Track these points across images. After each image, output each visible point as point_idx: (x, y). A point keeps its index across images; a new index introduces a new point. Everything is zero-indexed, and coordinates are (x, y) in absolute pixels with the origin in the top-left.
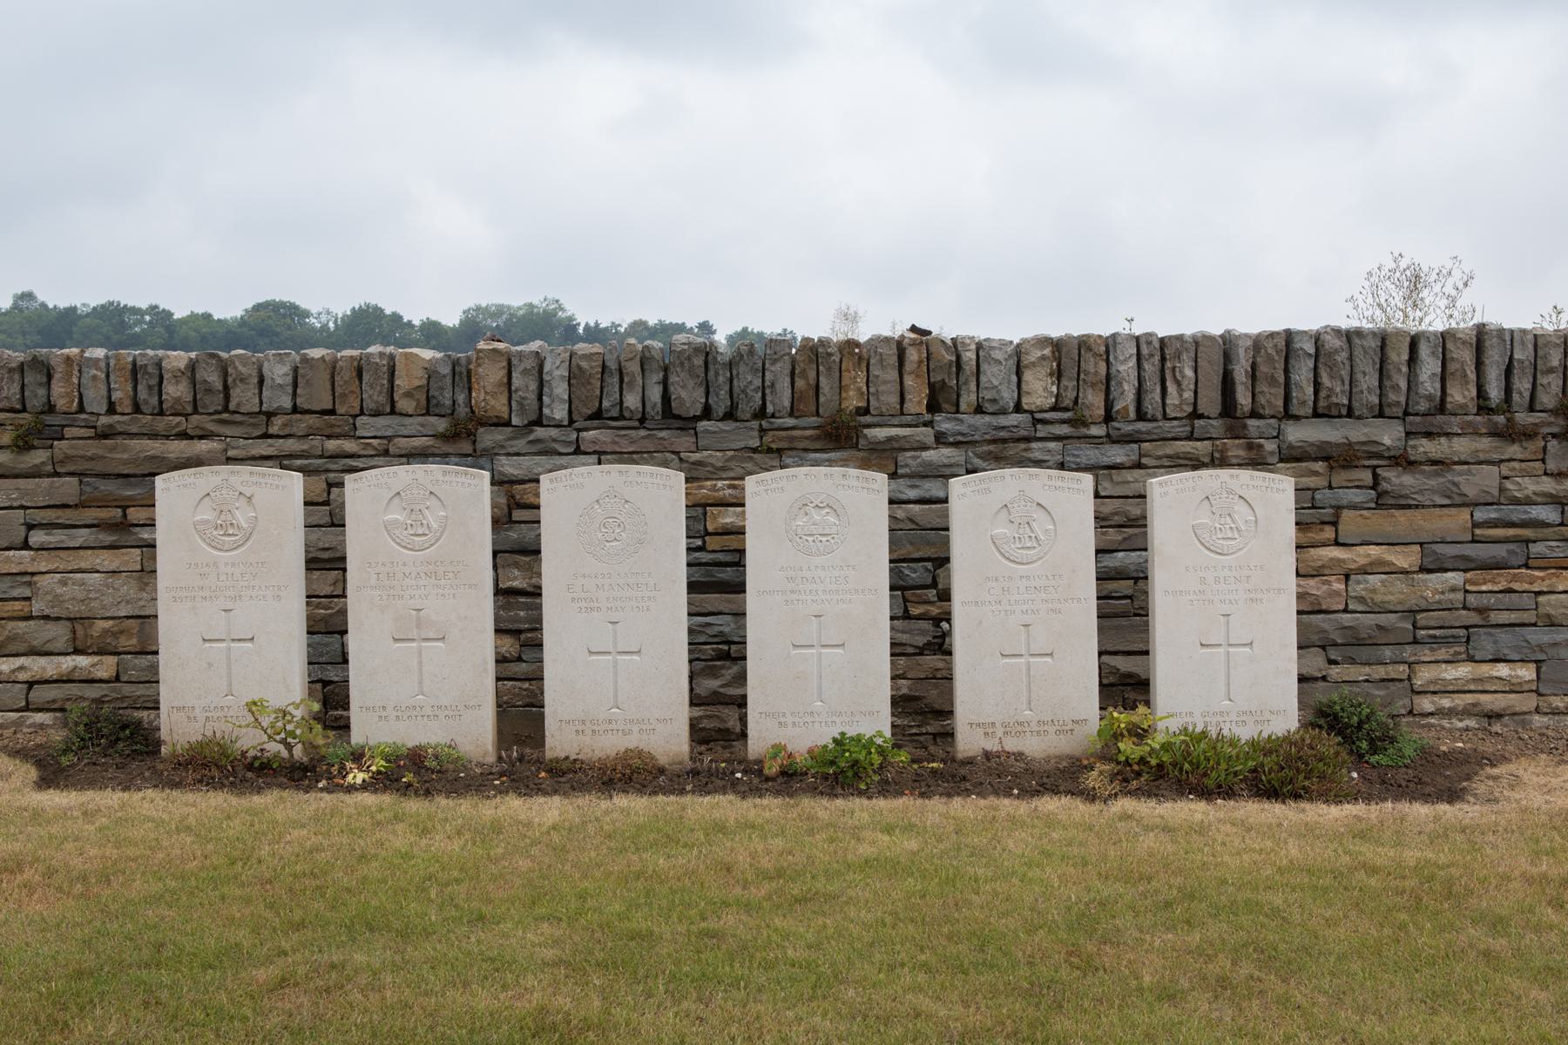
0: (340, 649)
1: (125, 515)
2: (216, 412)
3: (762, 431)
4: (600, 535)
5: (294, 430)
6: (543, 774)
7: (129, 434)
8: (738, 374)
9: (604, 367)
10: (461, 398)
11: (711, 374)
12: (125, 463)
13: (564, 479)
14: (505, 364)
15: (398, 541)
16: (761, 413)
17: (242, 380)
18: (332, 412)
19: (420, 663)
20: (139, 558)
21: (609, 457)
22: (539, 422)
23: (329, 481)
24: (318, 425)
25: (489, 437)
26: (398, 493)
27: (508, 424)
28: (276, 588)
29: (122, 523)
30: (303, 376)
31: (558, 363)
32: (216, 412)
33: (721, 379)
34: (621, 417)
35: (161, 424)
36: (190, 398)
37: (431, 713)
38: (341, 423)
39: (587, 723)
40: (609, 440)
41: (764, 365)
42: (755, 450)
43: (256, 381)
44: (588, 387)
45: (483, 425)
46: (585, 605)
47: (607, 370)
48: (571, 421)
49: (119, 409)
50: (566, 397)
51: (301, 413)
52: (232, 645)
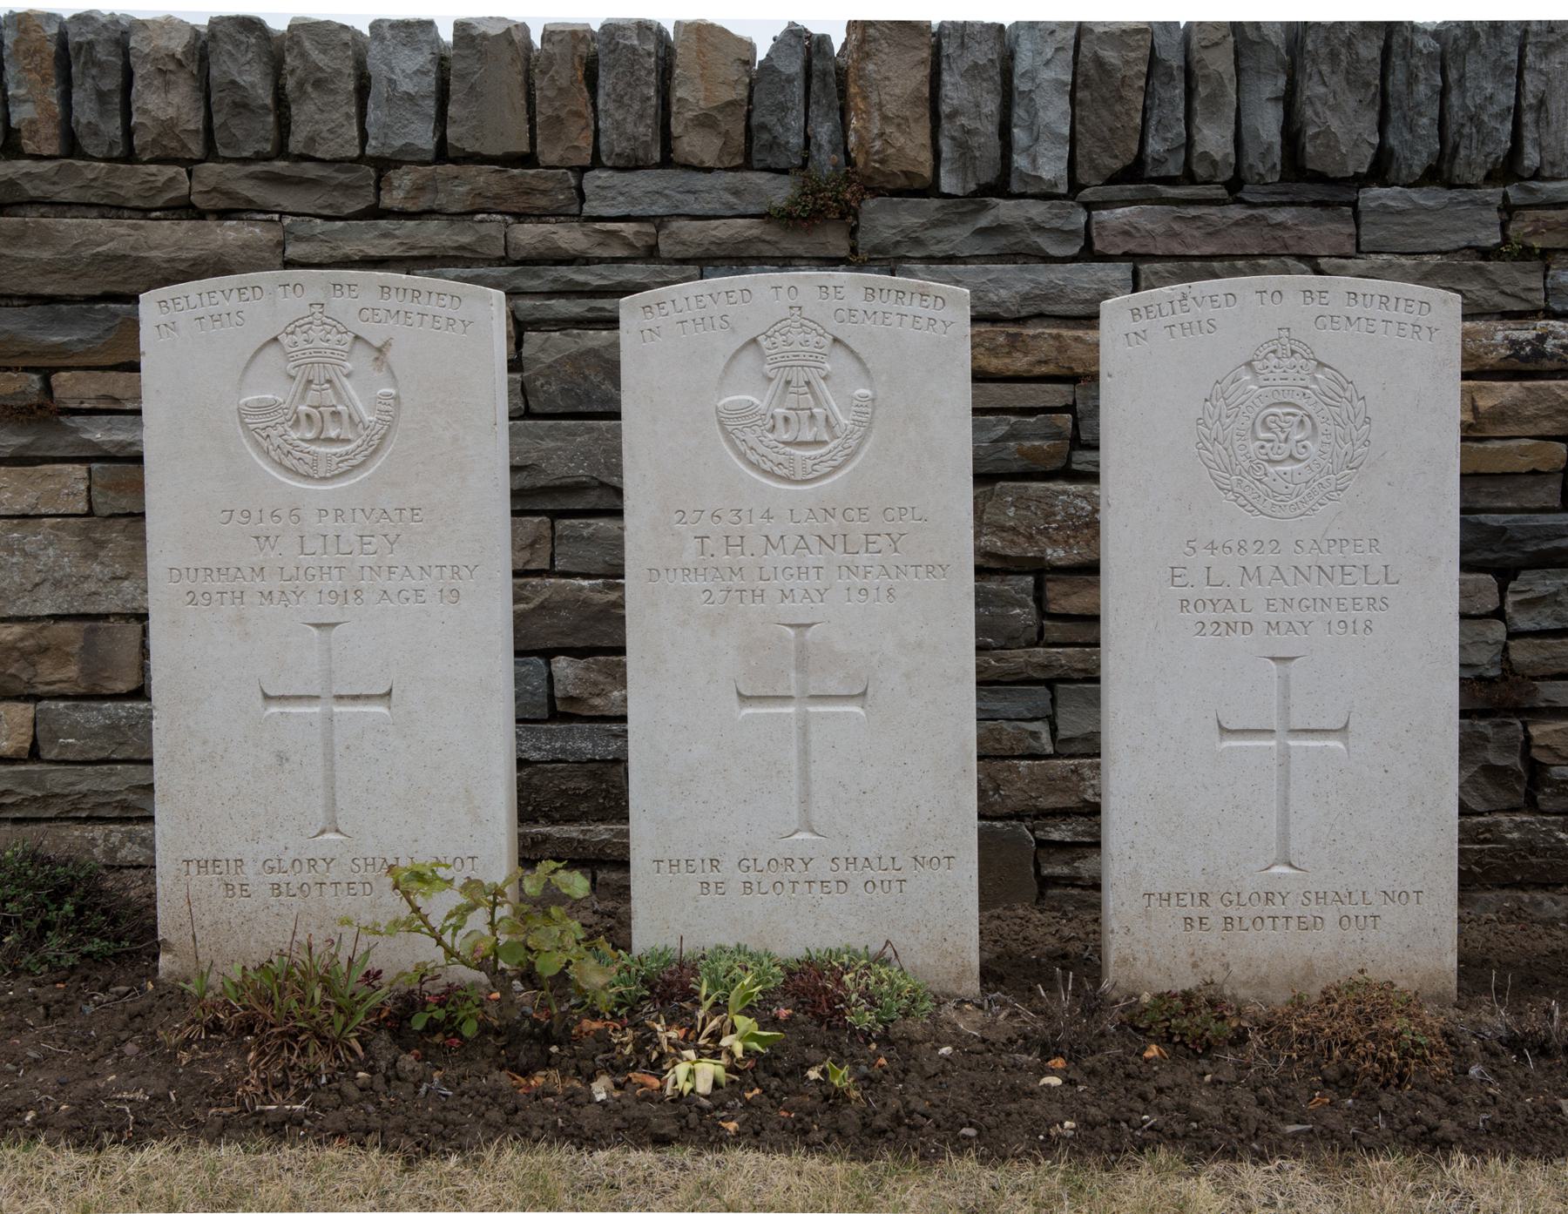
0: (544, 689)
1: (48, 389)
2: (260, 157)
3: (1508, 210)
4: (1253, 446)
5: (441, 200)
6: (1153, 1051)
7: (53, 204)
8: (1462, 77)
9: (1153, 60)
10: (824, 131)
11: (1398, 78)
12: (48, 269)
13: (1166, 308)
14: (925, 54)
15: (754, 457)
16: (1508, 169)
17: (318, 84)
18: (528, 160)
19: (804, 753)
20: (83, 487)
21: (1157, 266)
22: (1000, 187)
23: (520, 317)
24: (496, 189)
25: (889, 220)
26: (754, 341)
27: (930, 189)
28: (447, 572)
29: (40, 407)
30: (462, 77)
31: (1049, 53)
32: (260, 157)
33: (1422, 90)
34: (1189, 178)
35: (131, 182)
36: (195, 122)
37: (829, 876)
38: (550, 185)
39: (1214, 901)
40: (1159, 228)
41: (1522, 57)
42: (1486, 253)
43: (351, 87)
44: (1118, 108)
45: (877, 192)
46: (1214, 616)
47: (1160, 70)
48: (1075, 186)
49: (29, 146)
50: (1066, 130)
51: (455, 161)
52: (337, 709)
